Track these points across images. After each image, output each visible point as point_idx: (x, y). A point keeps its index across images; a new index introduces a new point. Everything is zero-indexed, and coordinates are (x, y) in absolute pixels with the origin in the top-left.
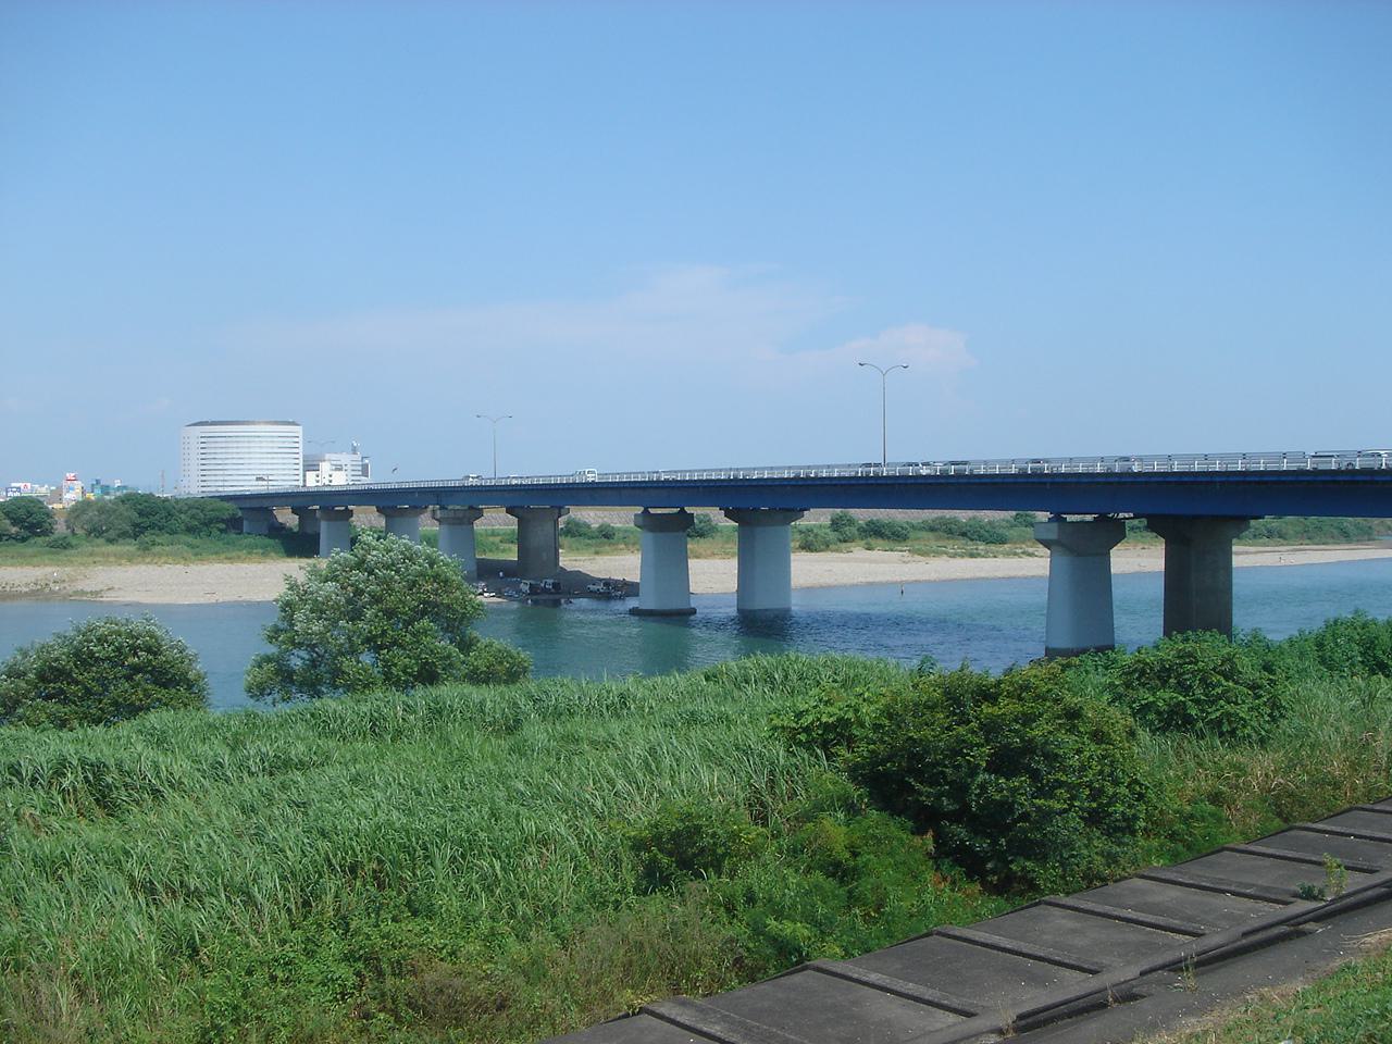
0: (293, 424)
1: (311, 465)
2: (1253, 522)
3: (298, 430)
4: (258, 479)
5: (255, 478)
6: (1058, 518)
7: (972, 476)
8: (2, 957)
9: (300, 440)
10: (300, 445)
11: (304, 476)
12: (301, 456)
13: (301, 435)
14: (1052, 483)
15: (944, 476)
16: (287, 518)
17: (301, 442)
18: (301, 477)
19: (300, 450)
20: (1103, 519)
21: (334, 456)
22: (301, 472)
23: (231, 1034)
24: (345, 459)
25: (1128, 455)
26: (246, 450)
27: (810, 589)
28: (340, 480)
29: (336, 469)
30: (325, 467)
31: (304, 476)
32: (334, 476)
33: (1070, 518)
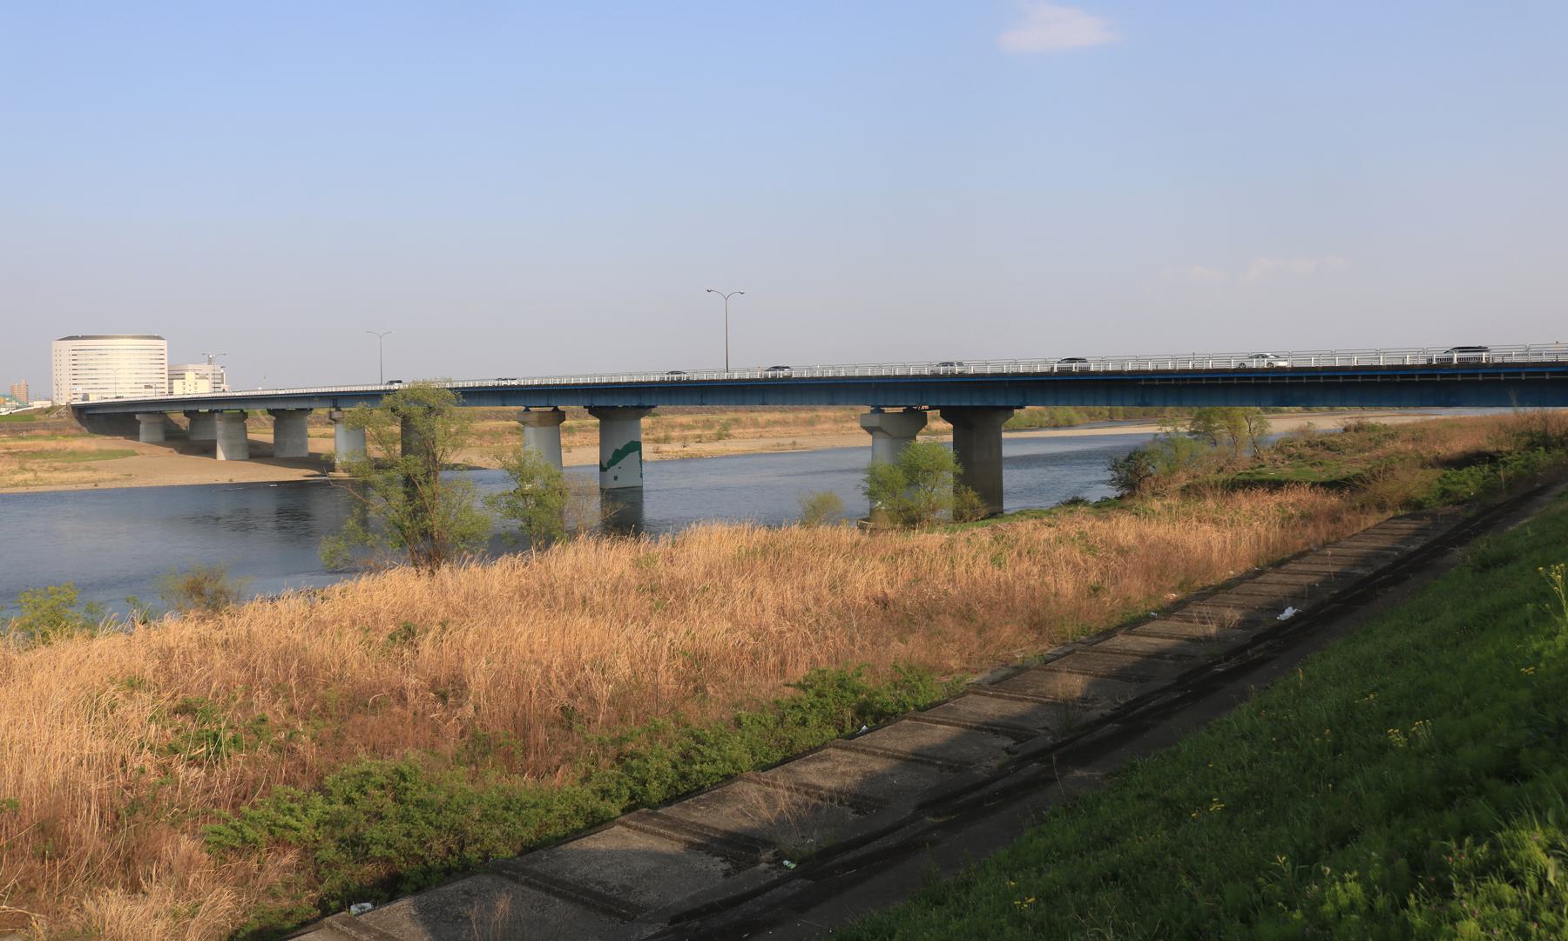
0: (158, 338)
1: (176, 374)
2: (1016, 411)
3: (163, 344)
4: (146, 387)
5: (143, 386)
6: (878, 410)
7: (688, 381)
8: (1110, 937)
9: (165, 352)
10: (165, 357)
11: (171, 384)
12: (166, 366)
13: (165, 348)
14: (1010, 382)
15: (1445, 365)
16: (179, 418)
17: (166, 355)
18: (166, 385)
19: (165, 361)
20: (909, 410)
21: (197, 367)
22: (166, 381)
23: (888, 939)
24: (206, 368)
25: (950, 360)
26: (105, 366)
27: (570, 467)
28: (204, 389)
29: (201, 378)
30: (190, 376)
31: (171, 384)
32: (193, 386)
33: (887, 410)
